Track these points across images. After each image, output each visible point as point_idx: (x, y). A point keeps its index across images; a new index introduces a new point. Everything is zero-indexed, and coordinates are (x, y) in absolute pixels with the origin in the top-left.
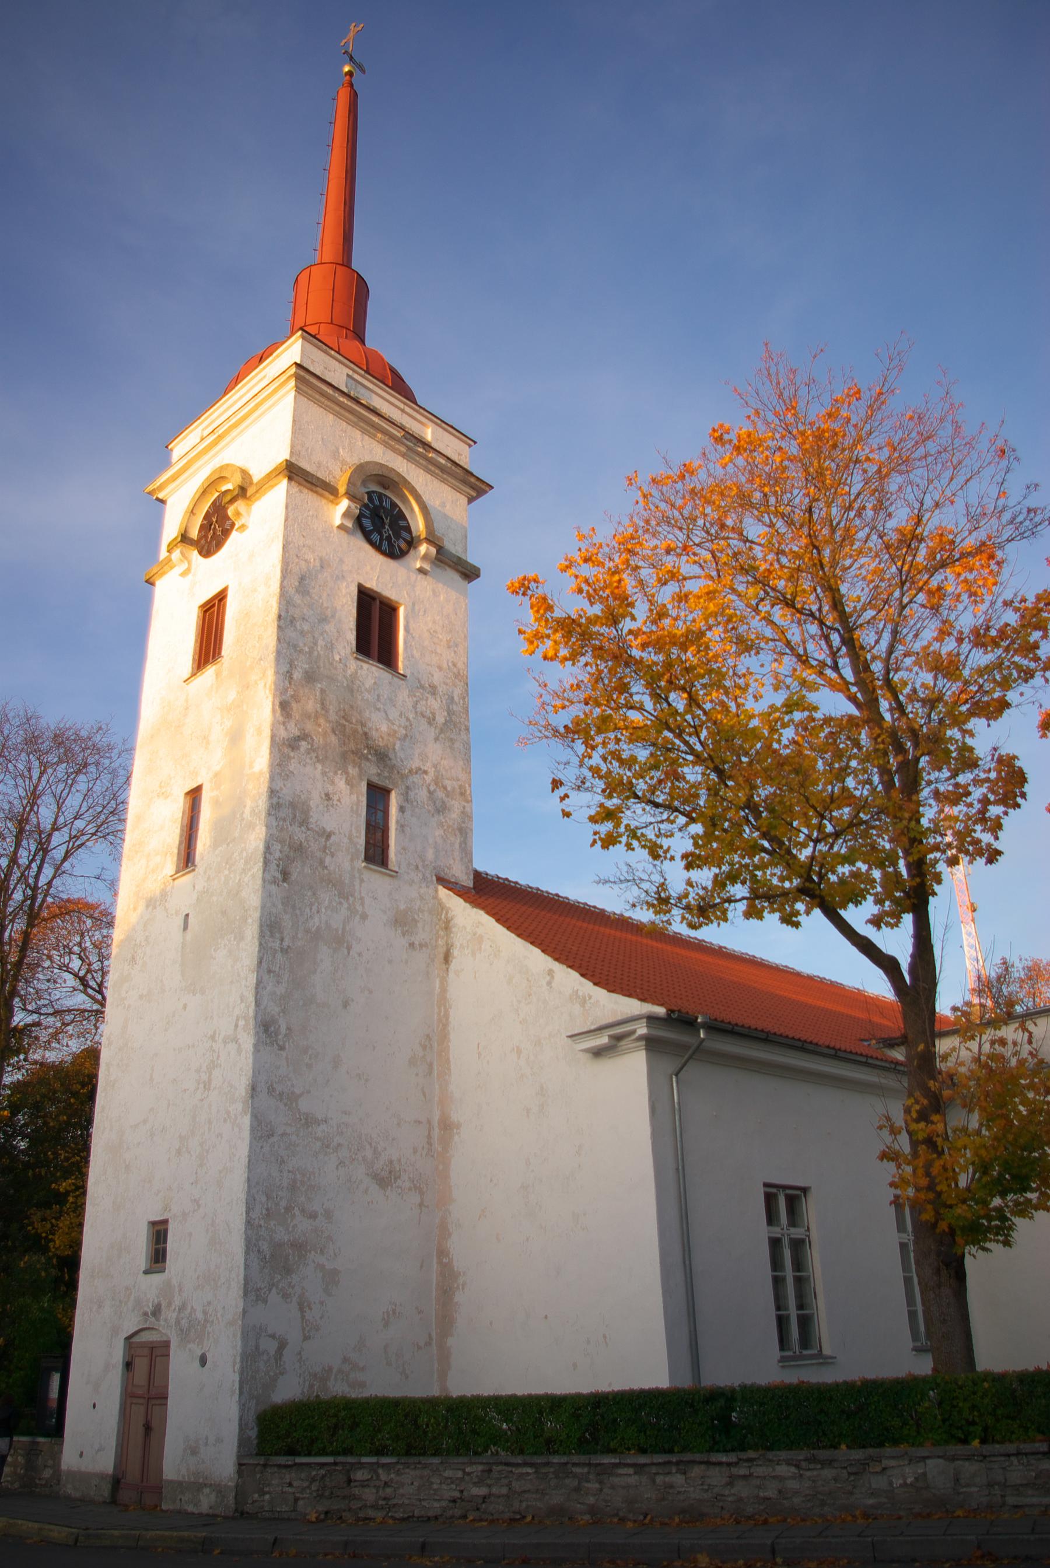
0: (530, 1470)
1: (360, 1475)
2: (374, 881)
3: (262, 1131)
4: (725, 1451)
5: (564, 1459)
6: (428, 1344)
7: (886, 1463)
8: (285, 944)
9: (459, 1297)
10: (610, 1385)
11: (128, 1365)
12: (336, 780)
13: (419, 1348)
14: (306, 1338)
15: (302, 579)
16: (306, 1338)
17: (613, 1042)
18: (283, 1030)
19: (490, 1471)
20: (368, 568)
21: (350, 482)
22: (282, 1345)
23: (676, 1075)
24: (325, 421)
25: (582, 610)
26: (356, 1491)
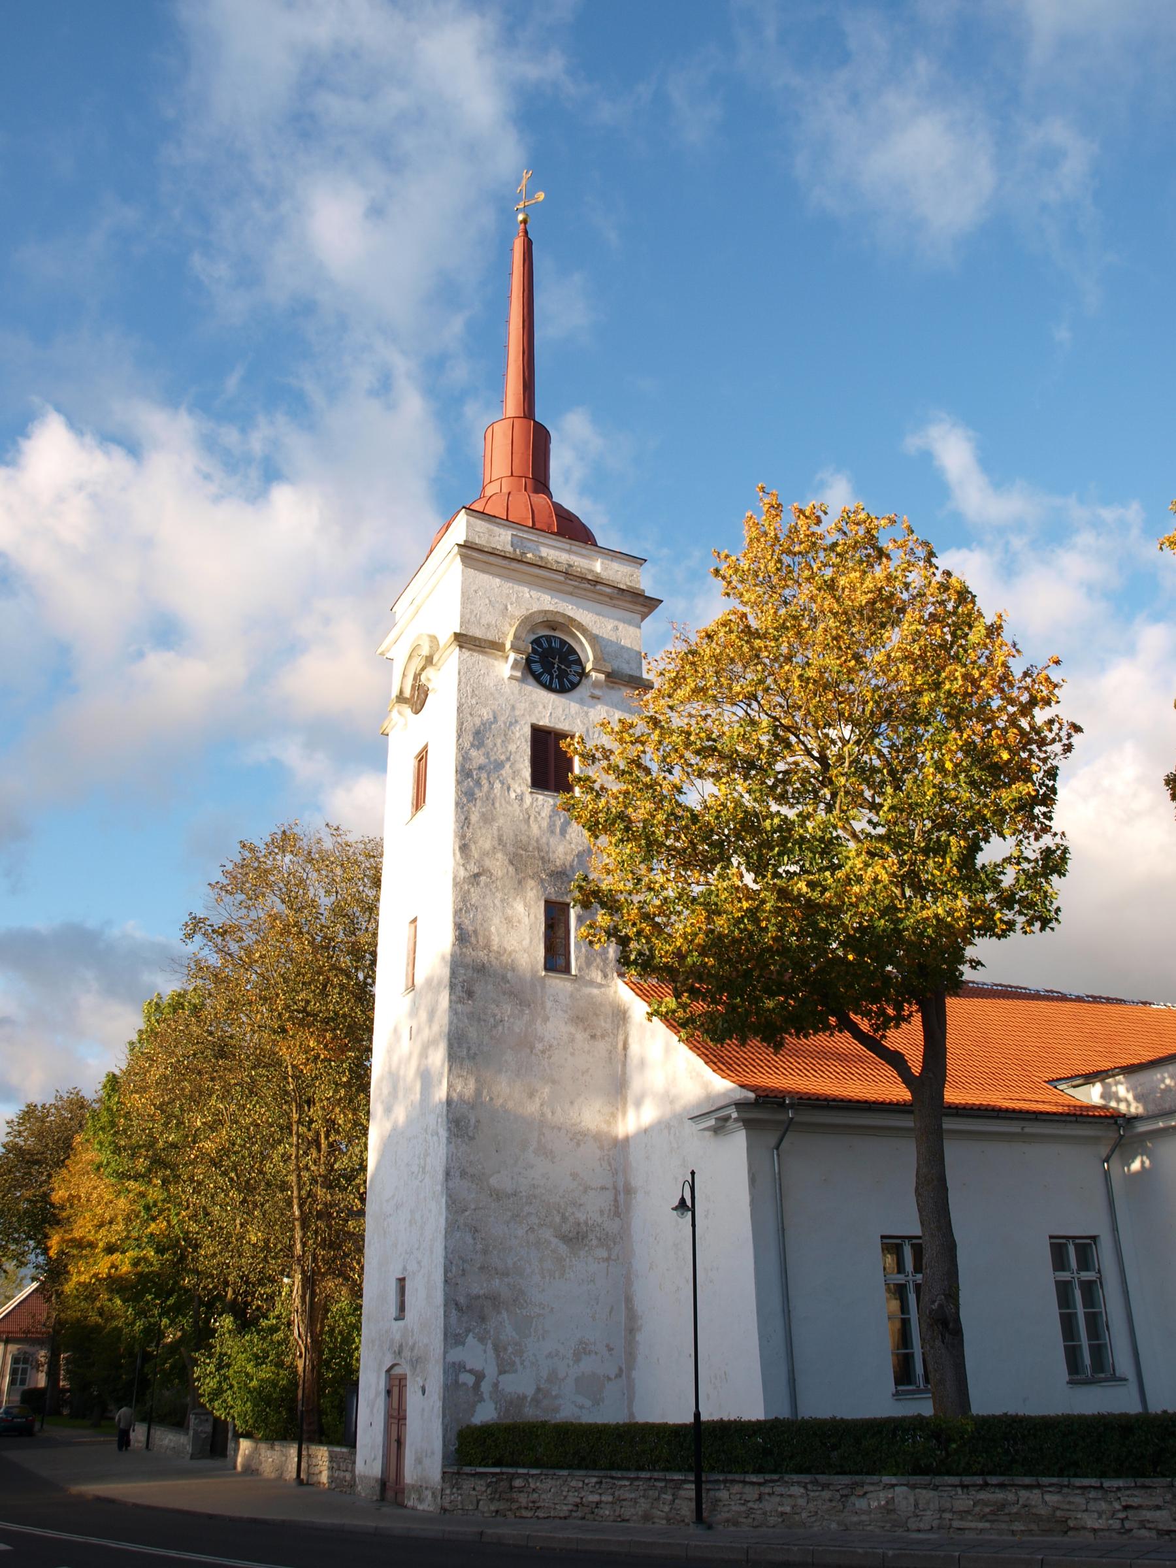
0: (627, 1483)
1: (518, 1483)
2: (557, 983)
3: (455, 1206)
4: (680, 1470)
5: (648, 1475)
6: (619, 1376)
7: (867, 1488)
8: (472, 1052)
9: (639, 1337)
10: (711, 1414)
11: (389, 1392)
12: (515, 905)
13: (609, 1379)
15: (477, 733)
17: (720, 1124)
18: (473, 1121)
19: (601, 1483)
20: (541, 707)
21: (516, 637)
22: (479, 1377)
23: (777, 1148)
24: (491, 583)
26: (515, 1495)
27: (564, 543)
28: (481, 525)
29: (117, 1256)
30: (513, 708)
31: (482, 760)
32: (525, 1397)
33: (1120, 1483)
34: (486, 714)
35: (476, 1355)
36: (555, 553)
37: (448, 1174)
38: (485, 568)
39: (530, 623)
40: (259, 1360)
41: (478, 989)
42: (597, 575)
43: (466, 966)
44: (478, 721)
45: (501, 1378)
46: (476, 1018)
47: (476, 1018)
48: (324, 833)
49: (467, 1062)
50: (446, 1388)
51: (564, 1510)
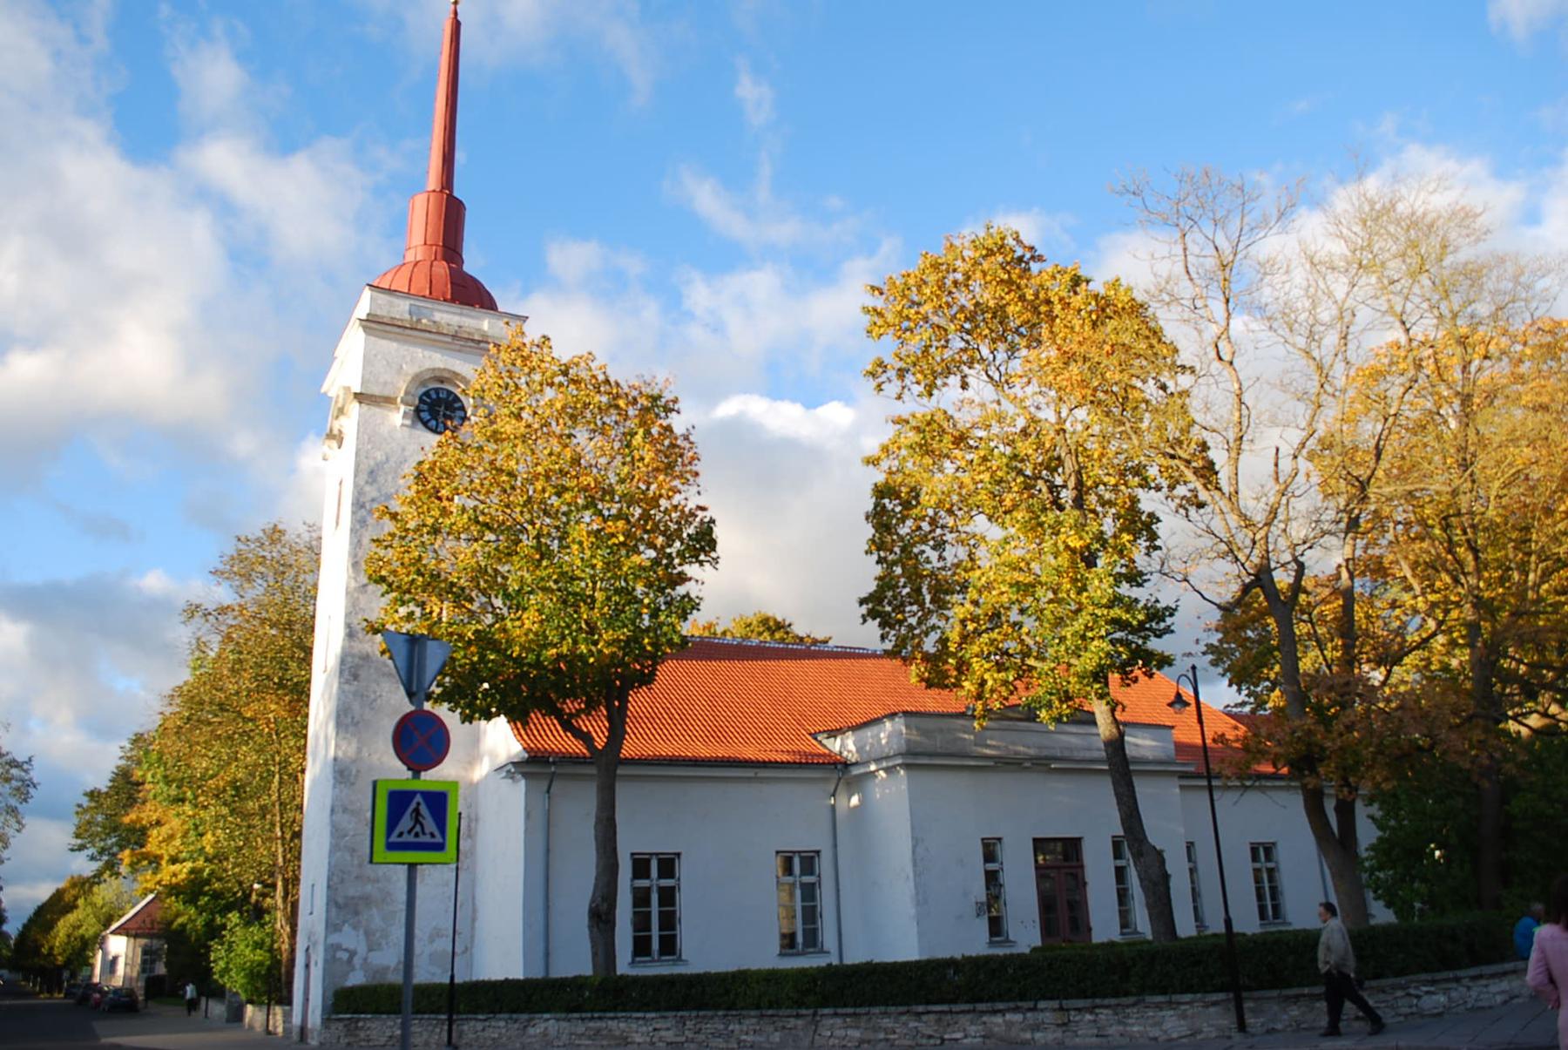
14: (370, 950)
16: (370, 950)
22: (353, 954)
25: (1168, 630)
27: (456, 308)
28: (383, 298)
29: (177, 867)
30: (403, 450)
31: (374, 494)
32: (388, 968)
33: (653, 1015)
34: (379, 456)
35: (350, 938)
36: (450, 317)
37: (332, 811)
38: (384, 335)
39: (418, 379)
40: (259, 945)
41: (363, 673)
42: (484, 335)
43: (353, 656)
44: (372, 463)
45: (371, 954)
46: (360, 695)
47: (360, 695)
48: (302, 529)
49: (351, 729)
50: (326, 961)
51: (383, 1040)
